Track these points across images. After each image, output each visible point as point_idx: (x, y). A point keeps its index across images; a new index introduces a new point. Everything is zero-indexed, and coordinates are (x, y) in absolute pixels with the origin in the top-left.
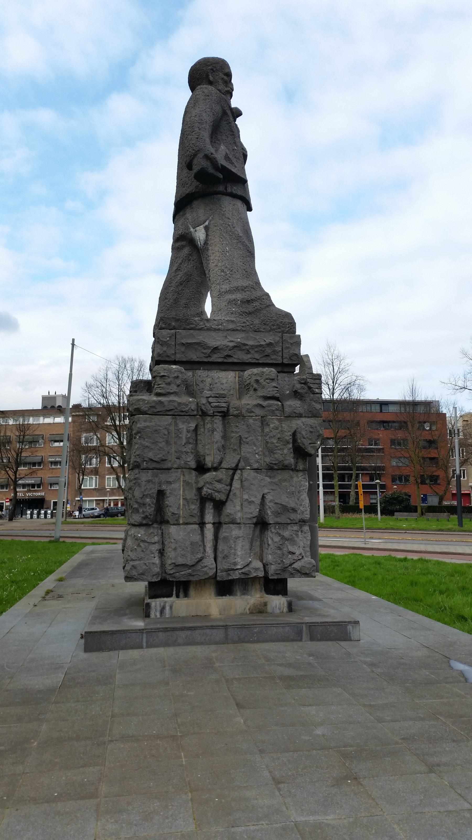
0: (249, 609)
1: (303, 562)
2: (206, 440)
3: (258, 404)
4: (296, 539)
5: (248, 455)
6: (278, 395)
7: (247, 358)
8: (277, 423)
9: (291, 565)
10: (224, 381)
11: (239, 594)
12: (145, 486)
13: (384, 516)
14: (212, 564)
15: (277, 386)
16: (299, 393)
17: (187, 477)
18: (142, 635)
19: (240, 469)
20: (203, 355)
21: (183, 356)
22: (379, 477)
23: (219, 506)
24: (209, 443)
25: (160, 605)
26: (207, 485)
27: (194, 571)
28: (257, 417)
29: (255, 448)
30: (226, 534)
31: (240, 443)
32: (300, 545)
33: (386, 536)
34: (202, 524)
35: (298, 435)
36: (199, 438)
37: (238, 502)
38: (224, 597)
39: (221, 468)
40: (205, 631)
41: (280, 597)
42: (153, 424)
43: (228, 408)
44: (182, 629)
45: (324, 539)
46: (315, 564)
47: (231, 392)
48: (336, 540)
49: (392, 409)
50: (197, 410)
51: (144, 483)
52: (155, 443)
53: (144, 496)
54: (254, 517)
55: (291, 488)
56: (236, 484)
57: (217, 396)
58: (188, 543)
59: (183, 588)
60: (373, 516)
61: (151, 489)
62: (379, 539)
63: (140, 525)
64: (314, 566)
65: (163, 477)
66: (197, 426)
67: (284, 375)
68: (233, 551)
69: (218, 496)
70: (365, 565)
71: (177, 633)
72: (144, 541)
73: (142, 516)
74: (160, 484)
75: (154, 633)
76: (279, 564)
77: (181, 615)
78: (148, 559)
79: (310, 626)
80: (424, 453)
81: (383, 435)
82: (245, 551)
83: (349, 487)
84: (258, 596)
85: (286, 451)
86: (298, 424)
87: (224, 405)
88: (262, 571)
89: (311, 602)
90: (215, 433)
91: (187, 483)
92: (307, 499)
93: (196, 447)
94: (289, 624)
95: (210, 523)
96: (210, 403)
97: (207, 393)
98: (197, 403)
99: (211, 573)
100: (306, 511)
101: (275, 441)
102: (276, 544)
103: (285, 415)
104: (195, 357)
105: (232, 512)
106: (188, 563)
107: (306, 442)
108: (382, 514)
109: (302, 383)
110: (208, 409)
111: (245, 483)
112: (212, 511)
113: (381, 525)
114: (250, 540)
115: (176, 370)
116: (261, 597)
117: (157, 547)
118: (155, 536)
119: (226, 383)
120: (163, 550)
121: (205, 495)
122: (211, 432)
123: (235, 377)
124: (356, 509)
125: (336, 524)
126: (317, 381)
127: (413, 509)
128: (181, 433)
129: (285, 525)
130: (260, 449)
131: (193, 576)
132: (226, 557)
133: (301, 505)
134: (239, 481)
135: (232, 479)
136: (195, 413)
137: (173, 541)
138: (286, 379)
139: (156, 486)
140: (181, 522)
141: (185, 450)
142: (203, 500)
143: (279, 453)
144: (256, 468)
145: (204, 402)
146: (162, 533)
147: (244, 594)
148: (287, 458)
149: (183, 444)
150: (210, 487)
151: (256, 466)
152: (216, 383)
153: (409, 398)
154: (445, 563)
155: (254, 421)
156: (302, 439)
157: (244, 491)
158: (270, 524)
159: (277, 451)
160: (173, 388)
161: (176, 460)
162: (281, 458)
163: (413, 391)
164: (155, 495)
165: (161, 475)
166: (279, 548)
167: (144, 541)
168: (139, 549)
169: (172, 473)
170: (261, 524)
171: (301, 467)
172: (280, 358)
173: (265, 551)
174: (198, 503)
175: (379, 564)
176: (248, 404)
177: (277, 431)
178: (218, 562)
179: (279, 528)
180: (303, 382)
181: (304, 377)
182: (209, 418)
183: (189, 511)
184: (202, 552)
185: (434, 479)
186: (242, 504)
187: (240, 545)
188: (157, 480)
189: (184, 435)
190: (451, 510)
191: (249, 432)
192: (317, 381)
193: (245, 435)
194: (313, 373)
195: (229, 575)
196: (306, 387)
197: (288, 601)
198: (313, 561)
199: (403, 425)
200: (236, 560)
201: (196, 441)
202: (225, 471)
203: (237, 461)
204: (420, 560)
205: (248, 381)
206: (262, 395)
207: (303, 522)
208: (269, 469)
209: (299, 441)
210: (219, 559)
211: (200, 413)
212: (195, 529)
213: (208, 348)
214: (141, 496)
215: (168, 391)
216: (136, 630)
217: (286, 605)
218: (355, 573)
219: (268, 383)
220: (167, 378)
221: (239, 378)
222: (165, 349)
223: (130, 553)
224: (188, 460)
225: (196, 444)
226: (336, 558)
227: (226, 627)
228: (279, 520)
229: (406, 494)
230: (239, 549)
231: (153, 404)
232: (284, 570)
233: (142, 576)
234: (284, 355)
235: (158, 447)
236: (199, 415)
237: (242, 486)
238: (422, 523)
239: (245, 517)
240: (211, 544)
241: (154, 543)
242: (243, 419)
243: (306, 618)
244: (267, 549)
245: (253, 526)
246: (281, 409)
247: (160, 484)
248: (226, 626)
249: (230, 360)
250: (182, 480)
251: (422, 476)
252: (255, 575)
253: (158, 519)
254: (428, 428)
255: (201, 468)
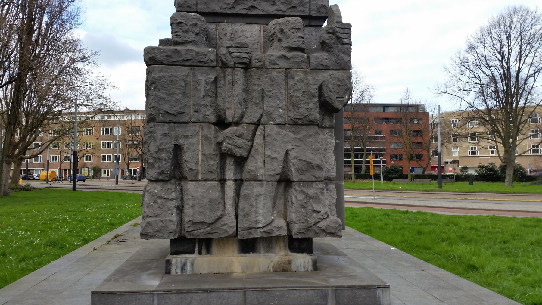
0: (273, 267)
1: (328, 221)
2: (227, 93)
3: (283, 55)
4: (321, 197)
5: (271, 110)
6: (303, 46)
7: (272, 10)
8: (302, 75)
9: (316, 224)
10: (248, 35)
11: (262, 251)
12: (161, 139)
13: (385, 182)
14: (232, 222)
15: (303, 36)
16: (327, 43)
17: (206, 132)
18: (153, 297)
19: (262, 124)
20: (226, 6)
21: (205, 7)
22: (382, 155)
23: (240, 162)
24: (229, 97)
25: (181, 261)
26: (227, 140)
27: (213, 229)
28: (281, 70)
29: (278, 102)
30: (247, 192)
31: (263, 97)
32: (326, 204)
33: (389, 194)
34: (222, 181)
35: (325, 89)
36: (219, 90)
37: (260, 159)
38: (247, 254)
39: (242, 123)
40: (222, 294)
41: (305, 255)
42: (169, 74)
43: (250, 60)
44: (197, 291)
45: (349, 196)
46: (341, 223)
47: (255, 46)
48: (357, 197)
49: (392, 110)
50: (217, 61)
52: (171, 94)
53: (159, 151)
54: (277, 174)
55: (316, 144)
56: (258, 140)
57: (238, 45)
58: (206, 201)
59: (206, 245)
60: (377, 181)
61: (167, 143)
62: (384, 196)
63: (157, 181)
64: (340, 225)
65: (180, 130)
66: (216, 78)
67: (311, 29)
68: (254, 209)
69: (239, 152)
70: (377, 216)
71: (191, 295)
72: (160, 197)
73: (158, 171)
74: (177, 138)
75: (165, 295)
76: (303, 223)
77: (202, 272)
78: (165, 216)
79: (336, 290)
80: (414, 140)
81: (385, 127)
82: (267, 209)
83: (361, 162)
84: (282, 253)
85: (311, 105)
86: (325, 77)
87: (245, 55)
88: (284, 230)
89: (336, 257)
90: (236, 85)
91: (206, 138)
92: (334, 157)
93: (216, 100)
94: (313, 288)
95: (231, 180)
96: (231, 53)
97: (229, 43)
98: (217, 54)
99: (232, 231)
100: (332, 169)
101: (300, 95)
102: (299, 202)
103: (311, 68)
104: (218, 8)
105: (254, 168)
106: (206, 221)
107: (334, 96)
108: (384, 180)
109: (330, 33)
110: (229, 60)
111: (268, 139)
112: (233, 167)
113: (384, 187)
114: (272, 198)
115: (195, 17)
116: (286, 255)
117: (175, 203)
118: (172, 192)
119: (251, 36)
120: (183, 207)
121: (225, 150)
122: (231, 85)
123: (260, 31)
124: (367, 176)
125: (352, 187)
126: (346, 31)
127: (406, 177)
128: (199, 85)
129: (310, 183)
130: (284, 103)
131: (212, 234)
132: (246, 215)
133: (327, 163)
134: (262, 137)
135: (254, 135)
136: (215, 64)
137: (190, 197)
138: (314, 33)
139: (173, 140)
140: (200, 178)
141: (204, 102)
142: (224, 156)
143: (304, 107)
144: (280, 122)
145: (224, 52)
146: (182, 189)
147: (268, 252)
148: (312, 113)
149: (202, 97)
150: (230, 142)
151: (279, 121)
152: (240, 37)
153: (404, 102)
154: (438, 215)
155: (277, 73)
156: (329, 93)
157: (266, 147)
158: (294, 181)
159: (302, 105)
160: (191, 37)
161: (194, 113)
162: (306, 113)
163: (407, 98)
164: (171, 150)
165: (177, 129)
166: (303, 207)
167: (160, 197)
168: (156, 206)
169: (190, 126)
170: (285, 181)
171: (327, 123)
172: (307, 10)
173: (289, 209)
174: (218, 159)
175: (388, 215)
176: (272, 55)
177: (302, 84)
178: (239, 219)
179: (303, 186)
180: (331, 31)
181: (333, 26)
182: (229, 70)
183: (208, 167)
184: (221, 209)
185: (419, 157)
186: (264, 161)
187: (262, 202)
188: (173, 134)
189: (202, 87)
190: (433, 177)
191: (272, 85)
192: (346, 31)
193: (267, 88)
194: (341, 22)
195: (250, 233)
196: (334, 37)
197: (312, 260)
198: (339, 220)
199: (399, 120)
200: (258, 218)
201: (216, 94)
202: (247, 126)
203: (259, 116)
204: (419, 213)
205: (272, 32)
206: (286, 45)
207: (329, 180)
208: (294, 125)
209: (326, 95)
210: (240, 217)
211: (220, 64)
212: (215, 186)
214: (157, 150)
215: (185, 39)
216: (147, 291)
217: (311, 263)
218: (374, 225)
219: (294, 33)
220: (184, 25)
221: (264, 31)
223: (146, 209)
224: (207, 113)
225: (216, 97)
226: (355, 211)
227: (244, 290)
228: (303, 177)
229: (400, 167)
230: (261, 207)
231: (169, 53)
232: (309, 229)
233: (158, 233)
234: (312, 7)
235: (174, 99)
236: (220, 67)
237: (264, 142)
238: (412, 186)
239: (267, 173)
240: (232, 201)
242: (265, 72)
243: (332, 280)
244: (291, 207)
245: (276, 183)
246: (306, 61)
247: (177, 138)
248: (245, 288)
249: (255, 12)
250: (200, 134)
251: (411, 155)
252: (278, 233)
253: (177, 175)
254: (416, 123)
255: (222, 123)
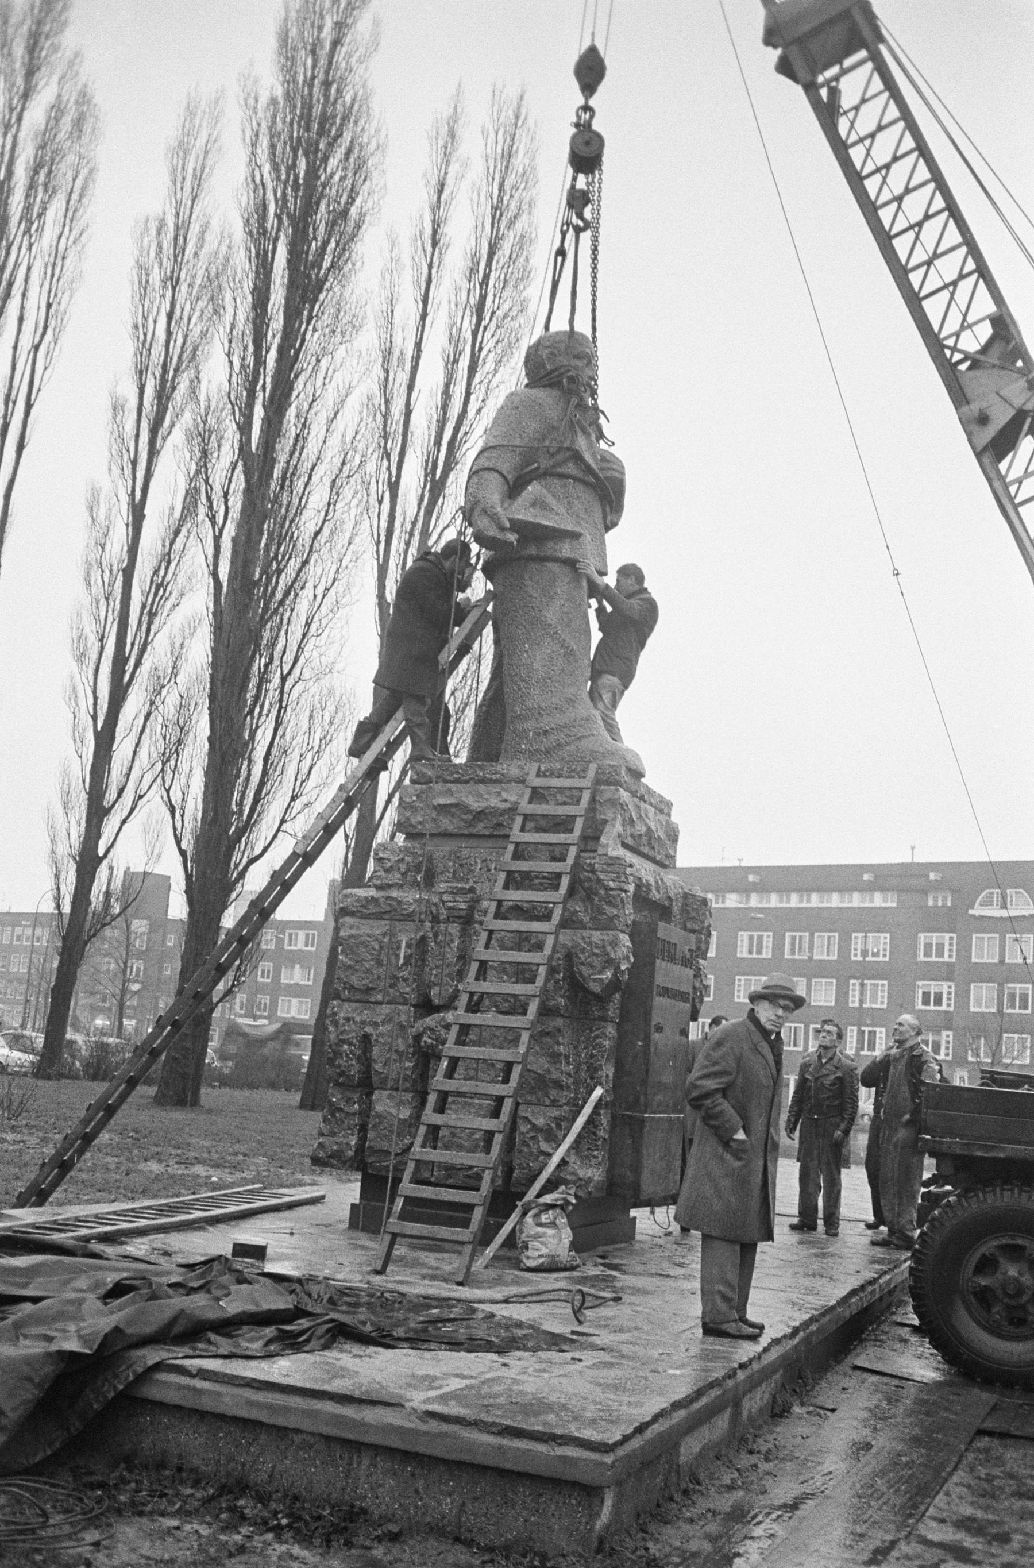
51: (341, 1021)
96: (444, 902)
213: (470, 811)
222: (408, 814)
241: (354, 1114)
